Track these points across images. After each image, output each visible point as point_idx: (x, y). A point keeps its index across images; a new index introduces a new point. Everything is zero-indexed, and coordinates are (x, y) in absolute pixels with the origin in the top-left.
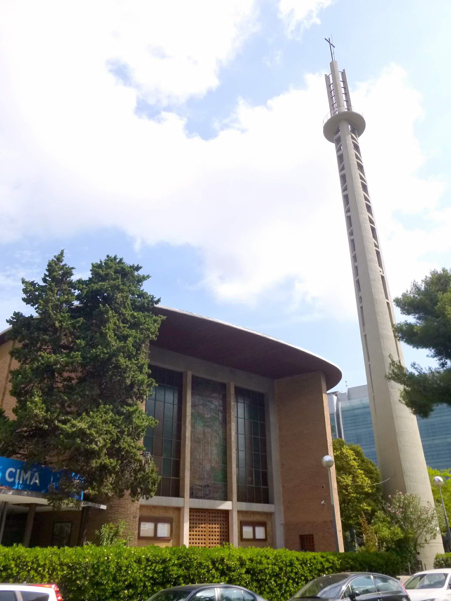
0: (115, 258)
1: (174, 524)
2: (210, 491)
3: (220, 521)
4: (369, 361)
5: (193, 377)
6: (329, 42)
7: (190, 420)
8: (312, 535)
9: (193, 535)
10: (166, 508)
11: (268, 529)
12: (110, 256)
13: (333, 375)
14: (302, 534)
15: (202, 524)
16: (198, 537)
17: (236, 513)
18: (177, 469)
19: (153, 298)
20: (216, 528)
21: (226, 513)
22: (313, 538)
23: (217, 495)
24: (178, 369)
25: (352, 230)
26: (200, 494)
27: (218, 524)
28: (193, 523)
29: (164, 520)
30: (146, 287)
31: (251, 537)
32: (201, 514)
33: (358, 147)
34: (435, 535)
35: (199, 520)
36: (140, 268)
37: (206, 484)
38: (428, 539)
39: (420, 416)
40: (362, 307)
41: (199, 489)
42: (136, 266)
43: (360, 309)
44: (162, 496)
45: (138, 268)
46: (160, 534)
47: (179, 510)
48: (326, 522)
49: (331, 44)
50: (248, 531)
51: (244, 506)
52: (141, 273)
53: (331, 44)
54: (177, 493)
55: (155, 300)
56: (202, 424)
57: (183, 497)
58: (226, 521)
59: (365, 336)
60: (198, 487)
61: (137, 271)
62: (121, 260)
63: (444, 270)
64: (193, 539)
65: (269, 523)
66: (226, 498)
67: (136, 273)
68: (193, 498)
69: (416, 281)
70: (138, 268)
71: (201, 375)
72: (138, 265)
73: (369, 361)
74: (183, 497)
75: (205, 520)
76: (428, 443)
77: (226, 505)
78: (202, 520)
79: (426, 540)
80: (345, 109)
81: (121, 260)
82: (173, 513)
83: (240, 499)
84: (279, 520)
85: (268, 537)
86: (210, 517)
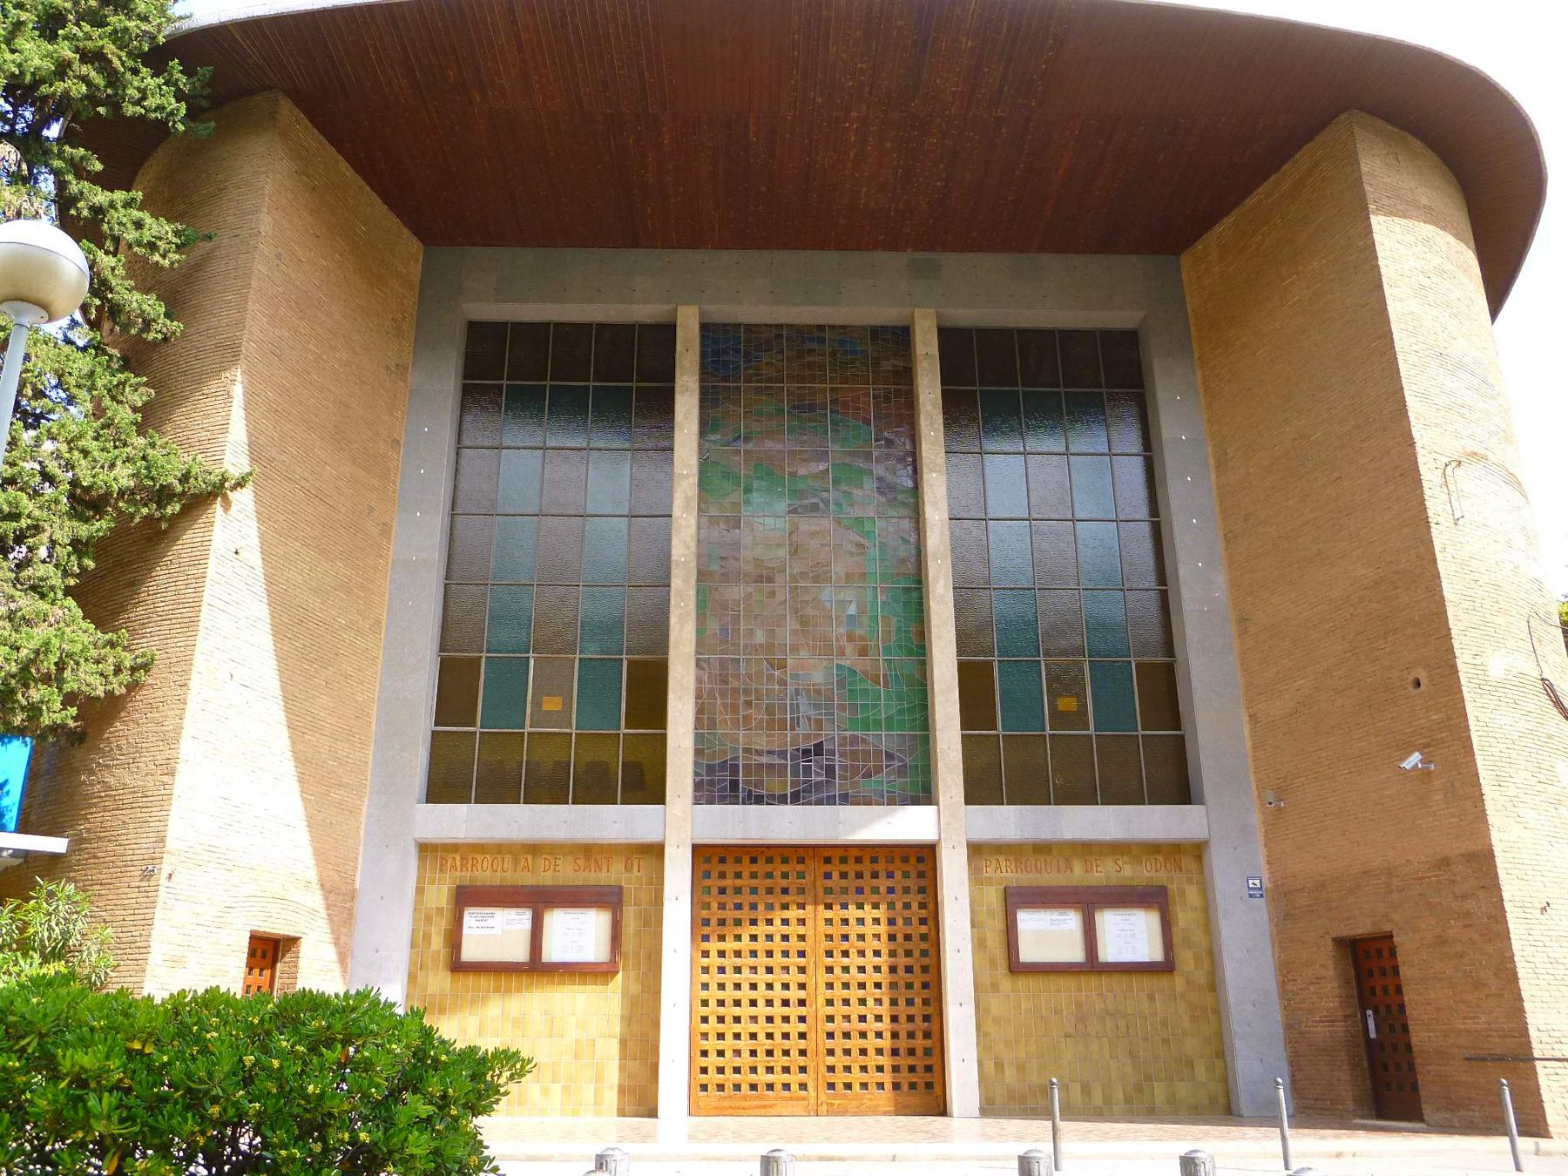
1: (630, 914)
5: (706, 329)
8: (1389, 937)
10: (589, 852)
11: (1184, 918)
14: (1345, 931)
15: (785, 907)
17: (962, 854)
20: (869, 922)
21: (920, 859)
22: (1393, 952)
23: (866, 787)
24: (644, 312)
26: (771, 784)
27: (876, 906)
31: (520, 954)
37: (811, 745)
41: (771, 767)
46: (553, 952)
47: (655, 852)
48: (1445, 862)
50: (1048, 934)
51: (1008, 822)
54: (646, 786)
56: (782, 506)
58: (922, 890)
60: (764, 760)
65: (1192, 894)
66: (924, 794)
68: (710, 802)
71: (753, 308)
75: (801, 891)
77: (905, 824)
82: (628, 869)
83: (982, 788)
86: (828, 876)
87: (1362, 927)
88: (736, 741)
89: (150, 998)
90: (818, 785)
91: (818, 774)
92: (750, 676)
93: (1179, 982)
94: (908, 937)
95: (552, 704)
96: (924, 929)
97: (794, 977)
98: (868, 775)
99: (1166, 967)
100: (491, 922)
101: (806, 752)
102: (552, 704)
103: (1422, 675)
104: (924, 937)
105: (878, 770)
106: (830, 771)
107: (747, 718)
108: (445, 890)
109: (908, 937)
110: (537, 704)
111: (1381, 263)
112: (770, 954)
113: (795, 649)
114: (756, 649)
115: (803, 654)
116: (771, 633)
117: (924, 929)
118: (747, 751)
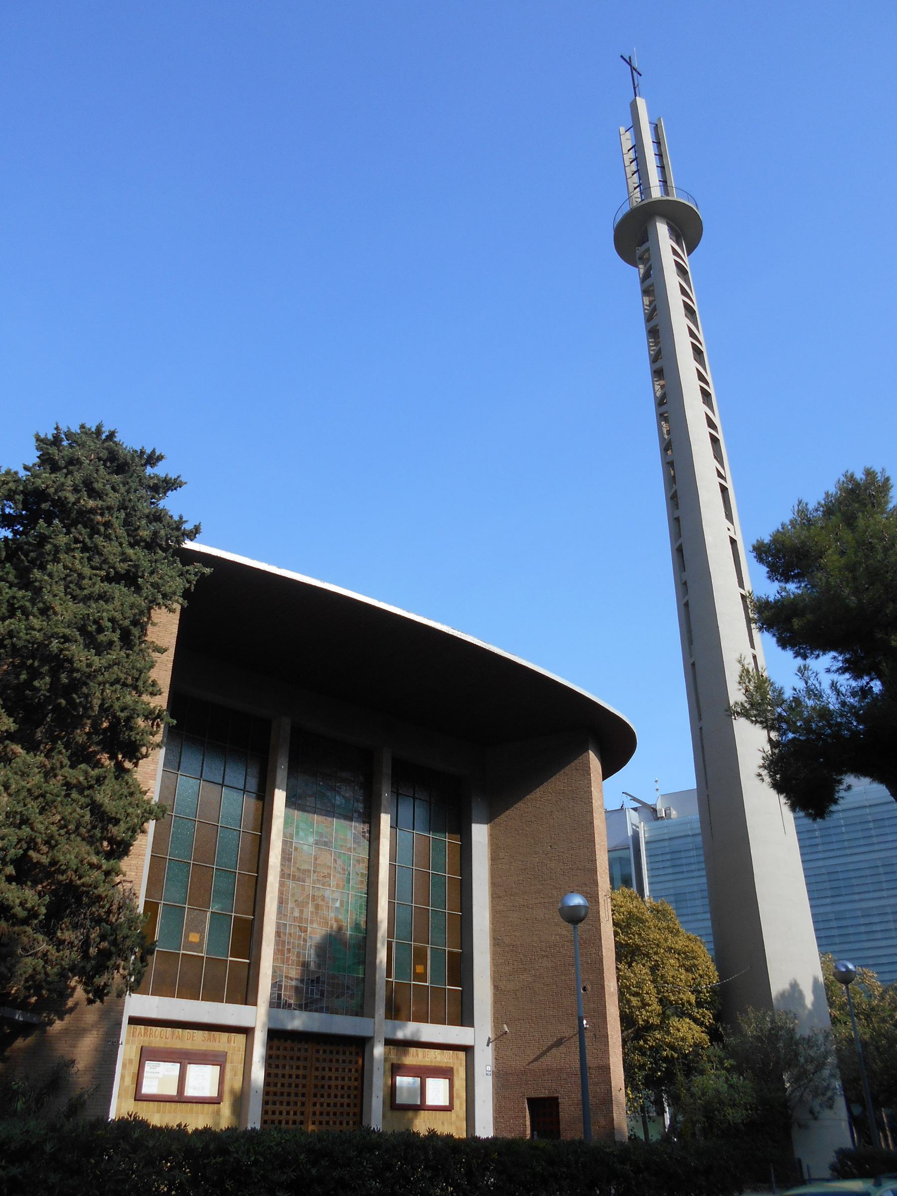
0: (99, 431)
1: (228, 1067)
2: (322, 994)
3: (344, 1061)
4: (700, 719)
6: (629, 63)
7: (281, 827)
8: (557, 1098)
9: (275, 1094)
12: (88, 426)
13: (615, 742)
16: (285, 1098)
18: (247, 937)
19: (181, 521)
25: (676, 492)
28: (277, 1066)
29: (203, 1058)
30: (172, 504)
31: (173, 1091)
32: (289, 1044)
33: (700, 379)
34: (831, 1099)
35: (292, 1058)
36: (160, 458)
38: (817, 1108)
39: (808, 815)
40: (686, 605)
42: (148, 451)
43: (683, 607)
44: (181, 996)
45: (153, 459)
46: (430, 1101)
49: (633, 69)
52: (160, 471)
53: (633, 69)
55: (188, 527)
57: (255, 1004)
59: (693, 664)
61: (153, 465)
62: (112, 435)
63: (869, 473)
64: (274, 1103)
67: (149, 470)
69: (804, 501)
70: (153, 459)
72: (154, 451)
73: (700, 719)
74: (255, 1004)
76: (822, 910)
78: (298, 1059)
79: (811, 1112)
80: (656, 193)
81: (112, 435)
84: (484, 1060)
85: (457, 1103)
86: (318, 1051)
87: (544, 1094)
88: (281, 971)
89: (418, 1134)
90: (317, 1000)
91: (317, 994)
92: (290, 934)
93: (453, 1115)
94: (349, 1088)
95: (194, 938)
96: (356, 1083)
97: (299, 1108)
98: (338, 997)
99: (448, 1109)
100: (158, 1069)
101: (313, 981)
102: (194, 938)
103: (589, 987)
104: (356, 1088)
105: (343, 994)
106: (322, 994)
107: (288, 958)
108: (134, 1047)
109: (349, 1088)
110: (202, 940)
111: (594, 801)
112: (289, 1095)
113: (312, 922)
114: (295, 919)
115: (315, 926)
116: (301, 912)
117: (356, 1083)
118: (286, 977)
